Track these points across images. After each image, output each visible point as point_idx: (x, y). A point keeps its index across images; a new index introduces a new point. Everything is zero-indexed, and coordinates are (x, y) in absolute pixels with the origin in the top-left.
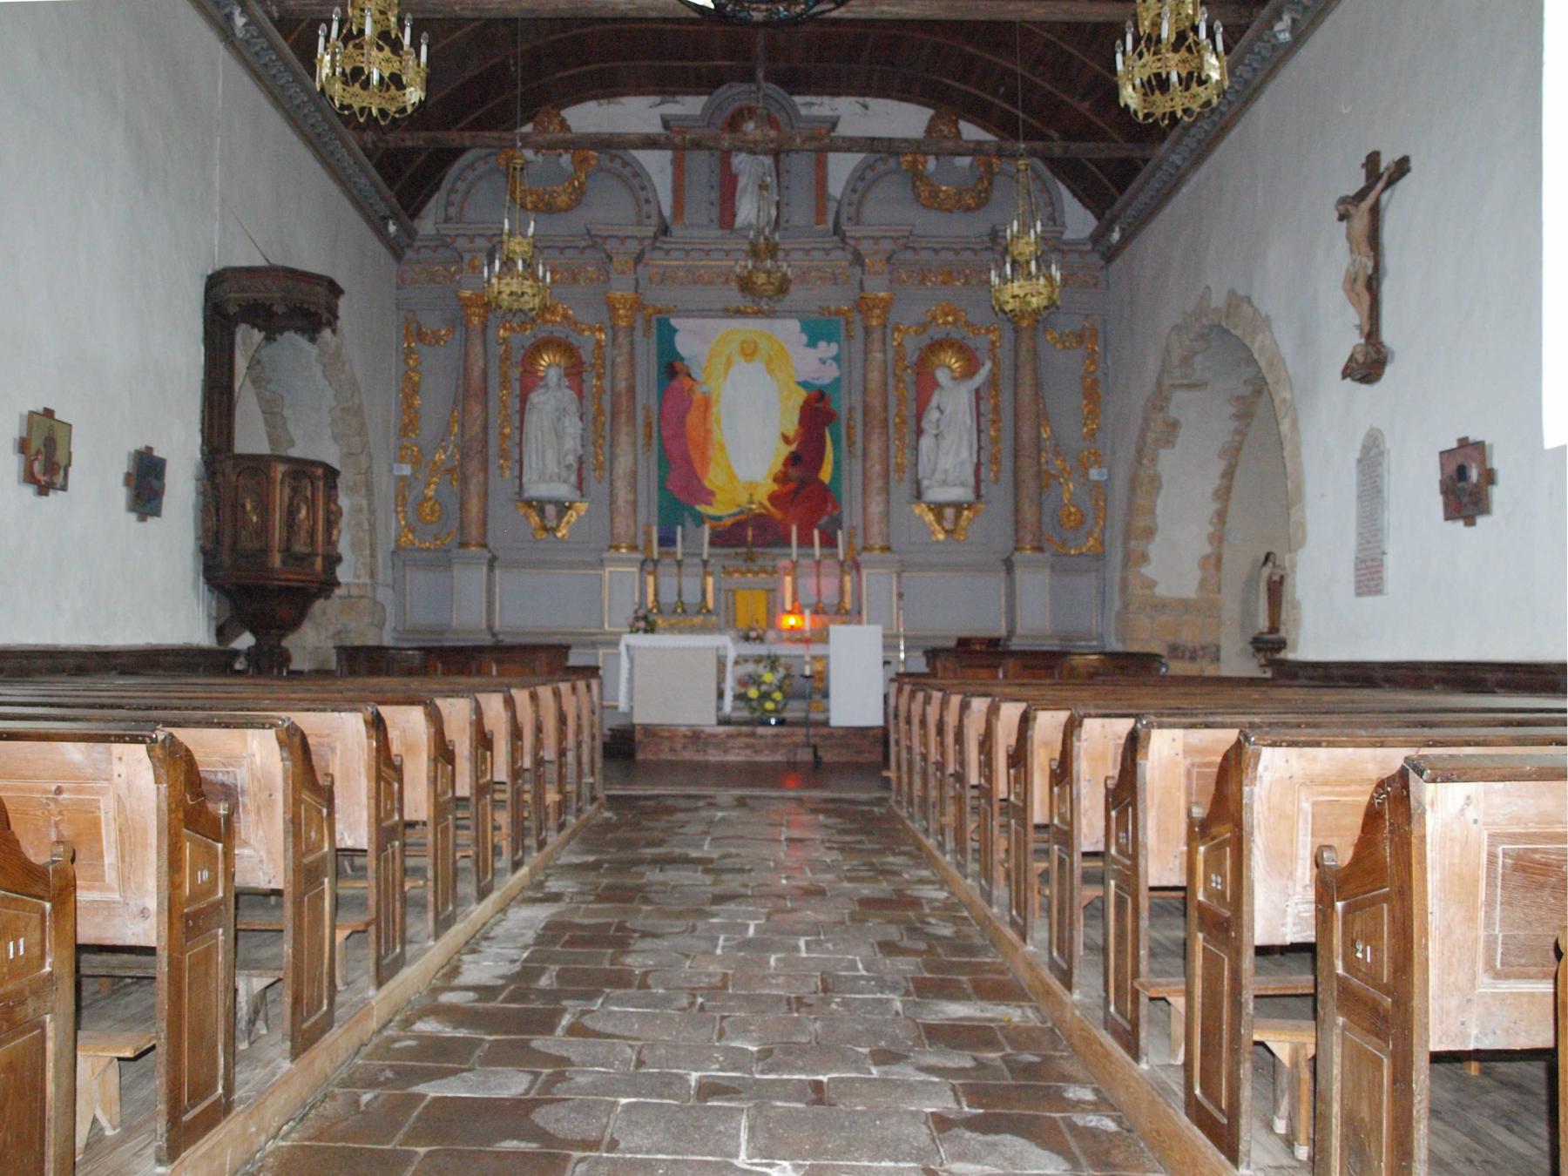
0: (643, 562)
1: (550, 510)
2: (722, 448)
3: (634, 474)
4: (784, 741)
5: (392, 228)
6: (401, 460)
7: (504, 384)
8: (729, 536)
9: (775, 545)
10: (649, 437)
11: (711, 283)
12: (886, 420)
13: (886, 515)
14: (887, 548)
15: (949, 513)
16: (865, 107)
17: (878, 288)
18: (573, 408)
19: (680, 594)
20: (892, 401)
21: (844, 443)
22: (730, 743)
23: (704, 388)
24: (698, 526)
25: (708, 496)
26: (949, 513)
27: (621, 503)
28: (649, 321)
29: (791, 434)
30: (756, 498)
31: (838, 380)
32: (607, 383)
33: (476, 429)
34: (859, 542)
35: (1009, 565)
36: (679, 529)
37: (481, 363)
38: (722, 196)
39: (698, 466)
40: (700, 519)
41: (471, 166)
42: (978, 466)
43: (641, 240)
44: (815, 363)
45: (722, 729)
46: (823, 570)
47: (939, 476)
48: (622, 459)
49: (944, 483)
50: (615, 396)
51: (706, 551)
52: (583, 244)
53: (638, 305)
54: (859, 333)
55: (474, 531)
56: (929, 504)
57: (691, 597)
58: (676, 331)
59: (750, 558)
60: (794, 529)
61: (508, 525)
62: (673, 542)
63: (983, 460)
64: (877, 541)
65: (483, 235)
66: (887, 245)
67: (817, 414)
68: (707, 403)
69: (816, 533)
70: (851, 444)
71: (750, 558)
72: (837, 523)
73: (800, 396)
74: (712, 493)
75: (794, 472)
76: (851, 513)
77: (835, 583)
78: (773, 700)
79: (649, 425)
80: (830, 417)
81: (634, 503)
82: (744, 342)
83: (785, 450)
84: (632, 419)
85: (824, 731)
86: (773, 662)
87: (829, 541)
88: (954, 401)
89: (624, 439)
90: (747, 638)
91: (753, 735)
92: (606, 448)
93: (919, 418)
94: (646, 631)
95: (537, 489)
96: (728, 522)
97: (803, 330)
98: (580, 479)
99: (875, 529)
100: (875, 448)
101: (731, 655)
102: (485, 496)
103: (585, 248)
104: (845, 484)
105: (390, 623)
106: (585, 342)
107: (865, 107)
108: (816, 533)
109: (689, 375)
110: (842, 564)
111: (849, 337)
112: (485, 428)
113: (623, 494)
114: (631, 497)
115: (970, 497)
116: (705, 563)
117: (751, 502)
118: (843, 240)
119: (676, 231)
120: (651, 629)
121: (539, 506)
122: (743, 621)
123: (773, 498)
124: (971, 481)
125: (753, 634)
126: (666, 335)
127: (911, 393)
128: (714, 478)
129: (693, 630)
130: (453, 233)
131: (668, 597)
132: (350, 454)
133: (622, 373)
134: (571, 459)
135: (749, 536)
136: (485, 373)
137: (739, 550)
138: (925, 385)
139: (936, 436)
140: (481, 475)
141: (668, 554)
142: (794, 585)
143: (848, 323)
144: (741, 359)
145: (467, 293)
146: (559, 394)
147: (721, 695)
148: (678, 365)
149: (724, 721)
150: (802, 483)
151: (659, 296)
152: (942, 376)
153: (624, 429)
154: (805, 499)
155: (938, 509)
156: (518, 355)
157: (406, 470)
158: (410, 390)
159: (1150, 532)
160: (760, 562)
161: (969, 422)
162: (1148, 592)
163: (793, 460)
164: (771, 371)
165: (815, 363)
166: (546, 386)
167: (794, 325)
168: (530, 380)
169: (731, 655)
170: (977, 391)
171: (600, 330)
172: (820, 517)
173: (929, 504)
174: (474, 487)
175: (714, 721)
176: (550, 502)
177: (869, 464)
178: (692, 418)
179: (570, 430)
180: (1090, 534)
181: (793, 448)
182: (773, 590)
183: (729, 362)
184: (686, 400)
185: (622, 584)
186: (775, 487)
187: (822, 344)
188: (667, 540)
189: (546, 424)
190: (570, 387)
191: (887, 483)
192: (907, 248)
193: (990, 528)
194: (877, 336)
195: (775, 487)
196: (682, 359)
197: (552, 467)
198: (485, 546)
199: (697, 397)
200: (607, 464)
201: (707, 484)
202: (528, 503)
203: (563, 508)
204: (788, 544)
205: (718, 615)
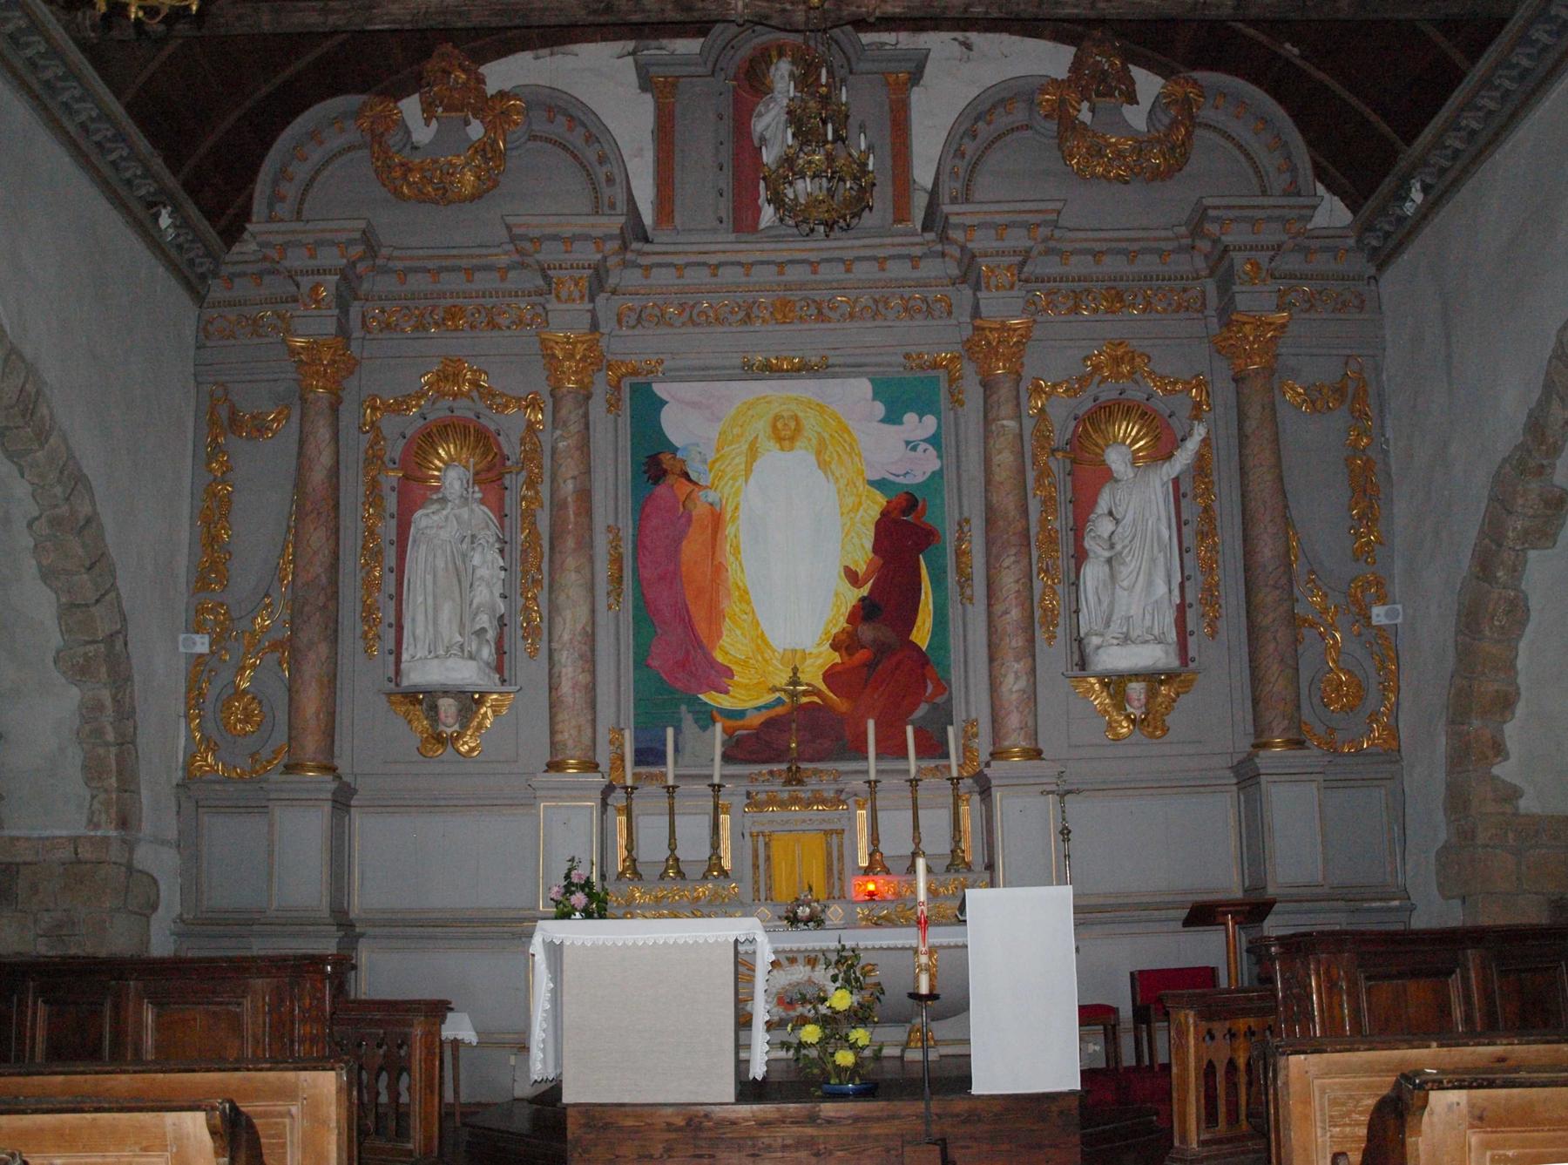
0: (608, 790)
1: (447, 706)
2: (744, 596)
3: (591, 638)
4: (876, 1129)
5: (165, 221)
6: (198, 628)
7: (374, 494)
8: (756, 744)
9: (841, 757)
10: (619, 580)
11: (720, 321)
12: (1025, 535)
13: (1031, 696)
14: (1035, 754)
15: (1136, 689)
16: (968, 46)
17: (1003, 307)
18: (489, 535)
19: (672, 847)
20: (1034, 506)
21: (952, 578)
22: (765, 1137)
23: (712, 496)
24: (704, 728)
25: (720, 677)
26: (1136, 689)
27: (566, 688)
28: (618, 387)
29: (861, 568)
30: (803, 677)
31: (938, 475)
32: (544, 490)
33: (318, 569)
34: (983, 746)
35: (1247, 777)
36: (670, 732)
37: (326, 459)
38: (737, 209)
39: (702, 628)
40: (707, 717)
41: (314, 136)
42: (1182, 609)
43: (599, 241)
44: (898, 450)
45: (745, 1110)
46: (922, 795)
47: (1116, 628)
48: (568, 614)
49: (1126, 639)
50: (558, 506)
51: (717, 771)
52: (504, 260)
53: (596, 360)
54: (973, 394)
55: (311, 745)
56: (1101, 677)
57: (693, 849)
58: (663, 403)
59: (794, 778)
60: (871, 724)
61: (373, 737)
62: (660, 758)
63: (1189, 598)
64: (1016, 740)
65: (333, 243)
66: (1018, 239)
67: (904, 534)
68: (716, 520)
69: (910, 730)
70: (965, 579)
71: (794, 778)
72: (944, 715)
73: (875, 504)
74: (729, 673)
75: (867, 632)
76: (970, 699)
77: (945, 816)
78: (853, 1047)
79: (617, 561)
80: (926, 537)
81: (591, 689)
82: (776, 418)
83: (852, 596)
84: (586, 545)
85: (959, 1106)
86: (847, 966)
87: (933, 747)
88: (1138, 506)
89: (572, 580)
90: (793, 920)
91: (812, 1119)
92: (543, 597)
93: (1078, 532)
94: (588, 915)
95: (424, 671)
96: (756, 720)
97: (876, 396)
98: (500, 651)
99: (1014, 720)
100: (1009, 581)
101: (765, 954)
102: (331, 683)
103: (509, 268)
104: (955, 643)
105: (171, 902)
106: (509, 425)
107: (968, 46)
108: (910, 730)
109: (686, 476)
110: (955, 782)
111: (957, 401)
112: (334, 566)
113: (570, 673)
114: (583, 678)
115: (1174, 663)
116: (716, 788)
117: (795, 682)
118: (944, 238)
119: (661, 237)
120: (598, 908)
121: (423, 700)
122: (784, 890)
123: (830, 676)
124: (1173, 636)
125: (804, 911)
126: (647, 409)
127: (1063, 494)
128: (730, 647)
129: (698, 909)
130: (279, 239)
131: (652, 849)
132: (73, 605)
133: (569, 468)
134: (484, 620)
135: (792, 741)
136: (335, 471)
137: (775, 767)
138: (1087, 480)
139: (1109, 561)
140: (324, 649)
141: (651, 777)
142: (881, 814)
143: (952, 380)
144: (772, 445)
145: (299, 342)
146: (465, 513)
147: (743, 1022)
148: (666, 459)
149: (749, 1090)
150: (881, 649)
151: (632, 346)
152: (1116, 459)
153: (571, 562)
154: (886, 672)
155: (1116, 683)
156: (395, 449)
157: (202, 644)
158: (214, 512)
159: (1506, 703)
160: (813, 784)
161: (1165, 533)
162: (1508, 809)
163: (865, 612)
164: (823, 465)
165: (898, 450)
166: (444, 501)
167: (863, 387)
168: (416, 489)
169: (765, 954)
170: (1176, 482)
171: (534, 405)
172: (915, 705)
173: (1101, 677)
174: (312, 669)
175: (728, 1092)
176: (446, 693)
177: (998, 608)
178: (691, 548)
179: (483, 572)
180: (1374, 717)
181: (865, 591)
182: (840, 832)
183: (753, 453)
184: (681, 520)
185: (568, 827)
186: (836, 658)
187: (910, 418)
188: (649, 755)
189: (440, 564)
190: (482, 501)
191: (1031, 640)
192: (1049, 252)
193: (1214, 715)
194: (1005, 391)
195: (836, 658)
196: (674, 450)
197: (450, 633)
198: (331, 769)
199: (699, 510)
200: (544, 626)
201: (719, 657)
202: (412, 696)
203: (469, 701)
204: (860, 752)
205: (739, 881)
